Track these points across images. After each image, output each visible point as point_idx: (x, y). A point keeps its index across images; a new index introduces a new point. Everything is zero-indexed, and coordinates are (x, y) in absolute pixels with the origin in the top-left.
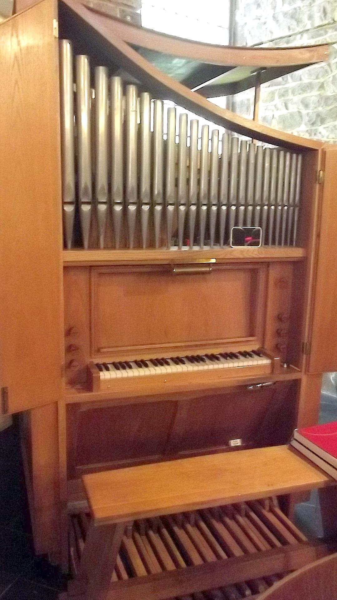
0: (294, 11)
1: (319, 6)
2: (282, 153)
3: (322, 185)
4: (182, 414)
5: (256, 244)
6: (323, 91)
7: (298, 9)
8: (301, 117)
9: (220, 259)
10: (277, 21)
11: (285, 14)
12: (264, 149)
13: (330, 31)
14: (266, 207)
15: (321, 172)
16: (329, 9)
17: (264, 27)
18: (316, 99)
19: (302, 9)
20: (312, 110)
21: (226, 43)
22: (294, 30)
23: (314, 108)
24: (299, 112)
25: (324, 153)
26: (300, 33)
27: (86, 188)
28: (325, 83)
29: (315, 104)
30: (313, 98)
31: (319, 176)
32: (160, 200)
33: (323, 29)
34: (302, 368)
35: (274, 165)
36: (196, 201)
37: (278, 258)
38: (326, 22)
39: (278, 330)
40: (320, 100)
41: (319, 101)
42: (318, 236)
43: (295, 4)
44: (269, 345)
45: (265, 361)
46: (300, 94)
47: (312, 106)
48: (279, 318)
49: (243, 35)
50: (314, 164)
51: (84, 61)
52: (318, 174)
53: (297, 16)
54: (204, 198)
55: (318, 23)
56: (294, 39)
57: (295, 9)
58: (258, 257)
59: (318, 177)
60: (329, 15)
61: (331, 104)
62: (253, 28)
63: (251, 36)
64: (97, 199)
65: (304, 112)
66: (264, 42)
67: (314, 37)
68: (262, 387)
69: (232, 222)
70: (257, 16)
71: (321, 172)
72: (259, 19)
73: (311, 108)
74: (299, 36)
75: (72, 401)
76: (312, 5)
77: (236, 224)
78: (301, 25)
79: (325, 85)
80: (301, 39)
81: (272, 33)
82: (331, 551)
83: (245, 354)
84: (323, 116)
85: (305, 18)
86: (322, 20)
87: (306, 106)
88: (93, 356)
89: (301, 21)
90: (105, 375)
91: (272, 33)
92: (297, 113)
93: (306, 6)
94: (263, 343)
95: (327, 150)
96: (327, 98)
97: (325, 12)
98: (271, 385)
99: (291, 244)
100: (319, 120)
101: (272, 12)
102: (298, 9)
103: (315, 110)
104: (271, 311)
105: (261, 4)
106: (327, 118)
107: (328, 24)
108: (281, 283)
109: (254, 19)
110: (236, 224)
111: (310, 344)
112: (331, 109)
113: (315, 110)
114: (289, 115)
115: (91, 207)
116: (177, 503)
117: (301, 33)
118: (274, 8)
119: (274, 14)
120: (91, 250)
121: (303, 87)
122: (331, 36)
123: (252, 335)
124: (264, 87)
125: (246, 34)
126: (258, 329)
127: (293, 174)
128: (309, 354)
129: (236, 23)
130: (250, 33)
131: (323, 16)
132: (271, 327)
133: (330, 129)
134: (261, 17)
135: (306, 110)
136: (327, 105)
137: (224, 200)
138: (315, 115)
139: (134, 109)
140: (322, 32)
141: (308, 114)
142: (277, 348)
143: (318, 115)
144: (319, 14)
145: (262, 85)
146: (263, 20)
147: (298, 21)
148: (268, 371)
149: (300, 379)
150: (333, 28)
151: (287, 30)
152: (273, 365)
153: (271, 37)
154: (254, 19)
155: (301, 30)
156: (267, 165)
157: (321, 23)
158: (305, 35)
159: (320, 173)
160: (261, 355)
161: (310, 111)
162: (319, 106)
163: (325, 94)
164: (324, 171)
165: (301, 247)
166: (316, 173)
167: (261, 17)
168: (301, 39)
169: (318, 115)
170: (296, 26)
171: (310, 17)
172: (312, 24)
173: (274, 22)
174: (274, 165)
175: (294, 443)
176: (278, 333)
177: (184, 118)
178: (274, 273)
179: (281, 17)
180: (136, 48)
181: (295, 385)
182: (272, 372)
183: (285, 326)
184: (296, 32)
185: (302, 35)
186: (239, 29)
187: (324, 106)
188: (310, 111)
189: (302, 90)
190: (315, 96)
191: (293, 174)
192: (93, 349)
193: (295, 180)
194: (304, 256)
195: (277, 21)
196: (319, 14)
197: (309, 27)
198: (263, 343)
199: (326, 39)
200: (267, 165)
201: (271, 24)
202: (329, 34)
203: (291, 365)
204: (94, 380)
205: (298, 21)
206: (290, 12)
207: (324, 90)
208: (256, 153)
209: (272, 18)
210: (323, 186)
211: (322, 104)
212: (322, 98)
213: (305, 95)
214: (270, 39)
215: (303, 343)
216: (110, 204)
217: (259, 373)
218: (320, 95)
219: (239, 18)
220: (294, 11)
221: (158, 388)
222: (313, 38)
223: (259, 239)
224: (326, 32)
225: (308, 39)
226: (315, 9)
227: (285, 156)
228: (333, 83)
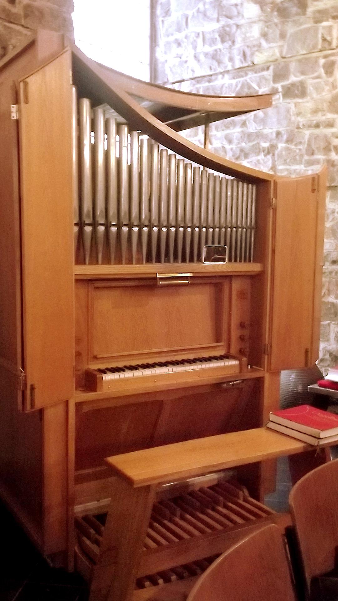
0: (215, 52)
1: (239, 49)
2: (235, 182)
3: (275, 211)
4: (165, 415)
5: (223, 260)
6: (244, 129)
7: (218, 50)
8: (225, 152)
9: (196, 273)
10: (199, 61)
11: (206, 55)
12: (220, 179)
13: (250, 73)
14: (234, 229)
15: (274, 199)
16: (248, 52)
17: (185, 65)
18: (239, 135)
19: (223, 51)
20: (236, 145)
21: (147, 79)
22: (215, 70)
23: (237, 143)
24: (223, 147)
25: (276, 184)
26: (221, 73)
27: (88, 212)
28: (247, 120)
29: (238, 140)
30: (236, 134)
31: (272, 202)
32: (147, 223)
33: (243, 70)
34: (265, 368)
35: (235, 194)
36: (175, 223)
37: (245, 271)
38: (246, 65)
39: (241, 336)
40: (243, 137)
41: (242, 137)
42: (273, 252)
43: (216, 46)
44: (233, 351)
45: (234, 362)
46: (223, 130)
47: (235, 141)
48: (242, 325)
49: (164, 71)
50: (267, 192)
51: (86, 103)
52: (271, 201)
53: (218, 57)
54: (182, 221)
55: (238, 65)
56: (216, 79)
57: (216, 50)
58: (226, 271)
59: (271, 204)
60: (249, 58)
61: (254, 140)
62: (174, 66)
63: (173, 73)
64: (98, 221)
65: (228, 147)
66: (186, 80)
67: (235, 77)
68: (233, 385)
69: (203, 241)
70: (177, 54)
71: (274, 199)
72: (180, 58)
73: (234, 144)
74: (220, 76)
75: (79, 400)
76: (232, 48)
77: (206, 243)
78: (222, 66)
79: (247, 123)
80: (222, 78)
81: (193, 71)
82: (337, 457)
83: (216, 358)
84: (247, 151)
85: (226, 60)
86: (242, 62)
87: (230, 142)
88: (89, 363)
89: (222, 63)
90: (108, 377)
91: (193, 71)
92: (221, 148)
93: (227, 48)
94: (229, 346)
95: (278, 181)
96: (249, 135)
97: (244, 55)
98: (239, 383)
99: (250, 261)
100: (243, 154)
101: (193, 52)
102: (218, 50)
103: (239, 146)
104: (235, 320)
105: (182, 44)
106: (250, 153)
107: (248, 67)
108: (242, 295)
109: (175, 57)
110: (206, 243)
111: (271, 346)
112: (254, 145)
113: (239, 146)
114: (213, 149)
115: (92, 228)
116: (194, 467)
117: (222, 73)
118: (195, 48)
119: (195, 54)
120: (103, 265)
121: (226, 124)
122: (251, 78)
123: (217, 341)
124: (213, 125)
125: (168, 71)
126: (225, 336)
127: (250, 201)
128: (270, 355)
129: (156, 60)
130: (171, 70)
131: (242, 59)
132: (235, 334)
133: (253, 163)
134: (182, 55)
135: (229, 145)
136: (250, 141)
137: (196, 222)
138: (238, 150)
139: (126, 145)
140: (243, 74)
141: (232, 149)
142: (241, 352)
143: (242, 150)
144: (239, 57)
145: (211, 124)
146: (184, 59)
147: (219, 62)
148: (237, 371)
149: (263, 377)
150: (252, 70)
151: (208, 69)
152: (241, 365)
153: (193, 75)
154: (175, 57)
155: (222, 71)
156: (229, 193)
157: (241, 66)
158: (226, 76)
159: (273, 200)
160: (229, 358)
161: (234, 146)
162: (242, 142)
163: (247, 131)
164: (276, 198)
165: (259, 262)
166: (270, 200)
167: (182, 55)
168: (222, 78)
169: (242, 150)
170: (217, 66)
171: (231, 59)
172: (233, 66)
173: (195, 62)
174: (235, 194)
175: (270, 425)
176: (242, 338)
177: (164, 153)
178: (236, 285)
179: (202, 57)
180: (131, 95)
181: (259, 381)
182: (241, 372)
183: (246, 332)
184: (217, 72)
185: (223, 75)
186: (160, 65)
187: (247, 142)
188: (234, 146)
189: (225, 126)
190: (238, 132)
191: (250, 201)
192: (89, 356)
193: (252, 206)
194: (262, 270)
195: (199, 61)
196: (239, 57)
197: (229, 68)
198: (229, 346)
199: (246, 81)
200: (229, 193)
201: (192, 63)
202: (249, 76)
203: (253, 367)
204: (98, 381)
205: (219, 62)
206: (211, 53)
207: (247, 127)
208: (176, 185)
209: (193, 58)
210: (276, 211)
211: (245, 140)
212: (244, 135)
213: (228, 131)
214: (192, 77)
215: (265, 345)
216: (107, 226)
217: (231, 372)
218: (243, 132)
219: (159, 54)
220: (215, 52)
221: (149, 386)
222: (234, 78)
223: (225, 255)
224: (246, 74)
225: (229, 79)
226: (235, 52)
227: (243, 187)
228: (254, 121)
